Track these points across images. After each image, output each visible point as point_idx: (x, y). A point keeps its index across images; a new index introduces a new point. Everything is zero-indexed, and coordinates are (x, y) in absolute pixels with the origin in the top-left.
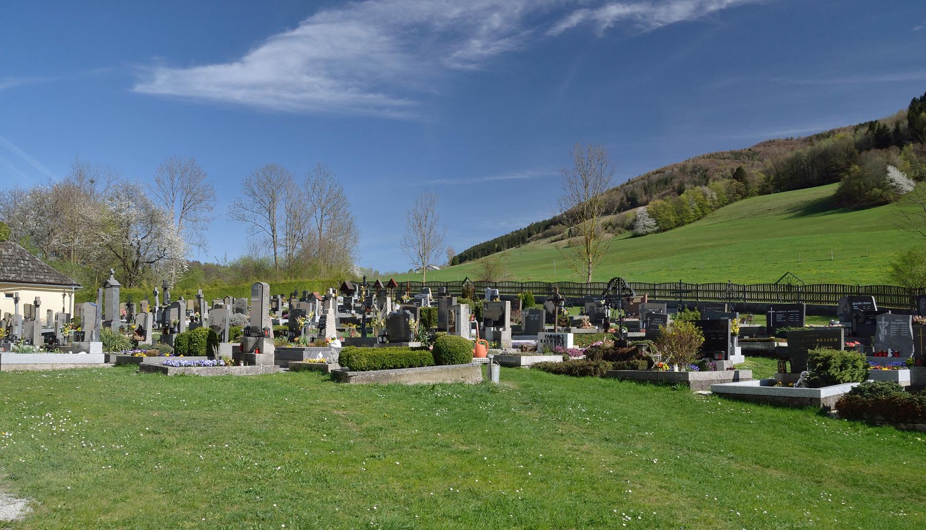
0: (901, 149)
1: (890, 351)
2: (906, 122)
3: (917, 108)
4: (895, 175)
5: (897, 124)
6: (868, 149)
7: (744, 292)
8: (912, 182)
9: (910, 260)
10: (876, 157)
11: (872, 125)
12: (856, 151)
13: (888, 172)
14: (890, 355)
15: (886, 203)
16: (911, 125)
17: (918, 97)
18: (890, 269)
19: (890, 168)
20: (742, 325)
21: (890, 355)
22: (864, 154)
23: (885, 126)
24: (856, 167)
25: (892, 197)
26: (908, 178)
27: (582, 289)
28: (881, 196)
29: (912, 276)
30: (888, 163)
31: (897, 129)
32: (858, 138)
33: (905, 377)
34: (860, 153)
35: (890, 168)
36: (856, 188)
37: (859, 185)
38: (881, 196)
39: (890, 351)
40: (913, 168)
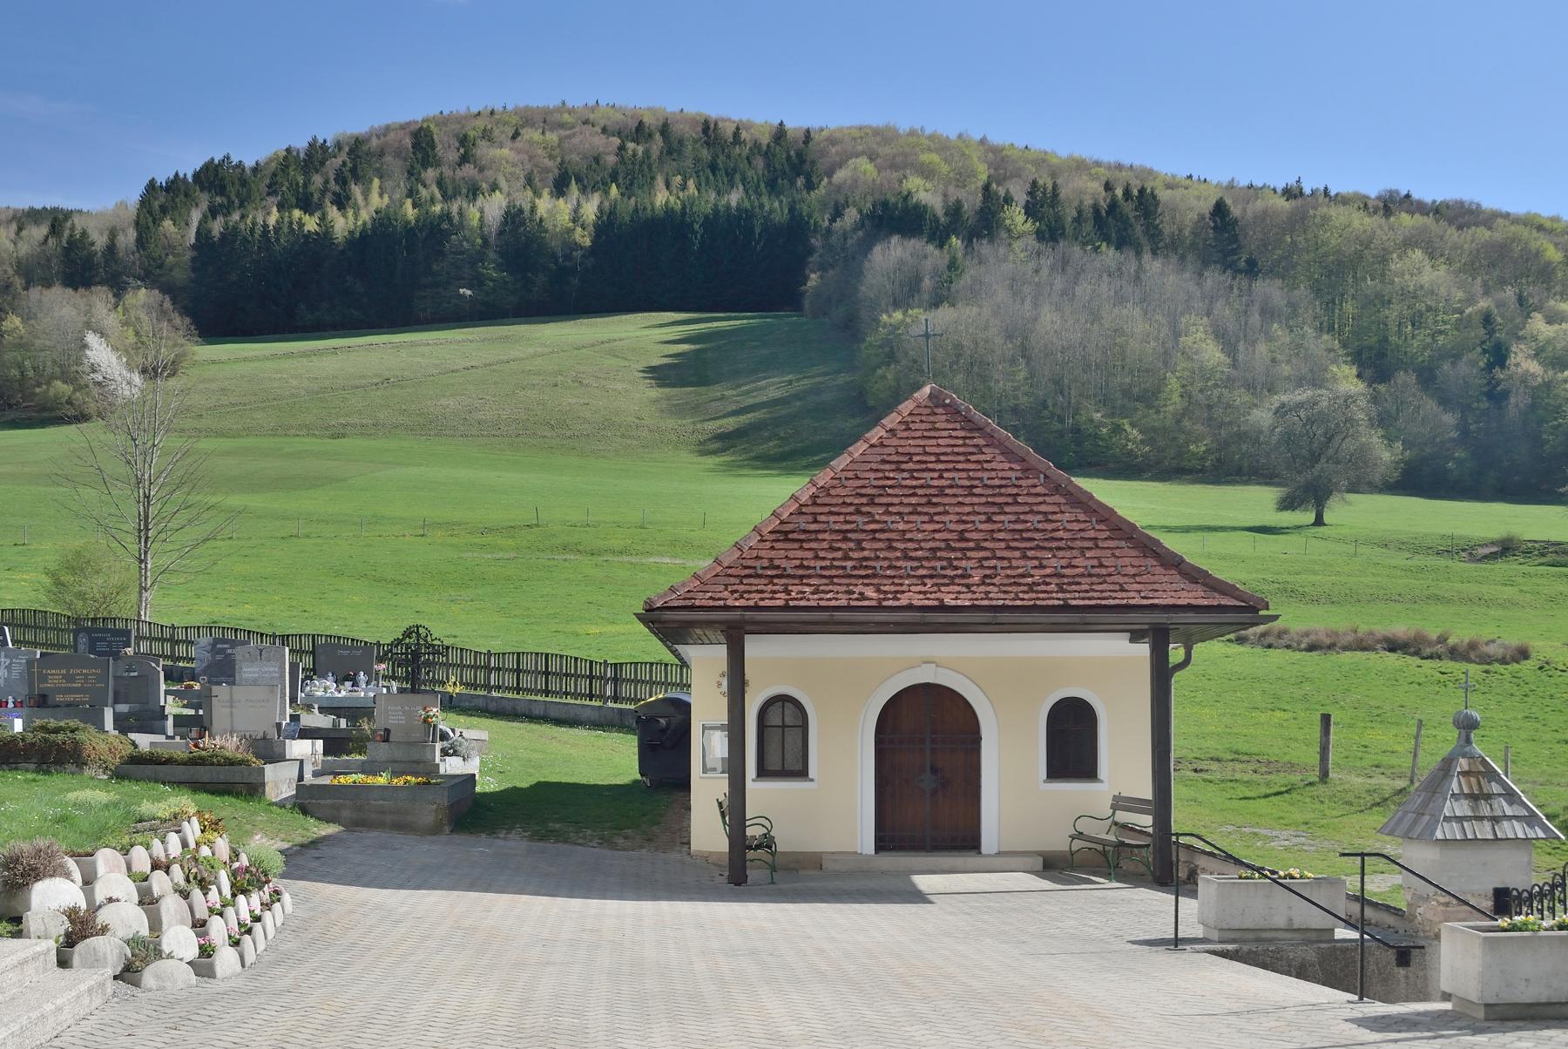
0: (118, 296)
1: (11, 700)
2: (132, 234)
3: (156, 204)
4: (101, 354)
5: (113, 234)
6: (48, 284)
7: (174, 642)
8: (137, 379)
9: (78, 565)
10: (60, 306)
11: (57, 220)
12: (18, 282)
13: (85, 346)
14: (11, 705)
15: (82, 418)
16: (141, 242)
17: (161, 179)
18: (47, 580)
19: (91, 338)
20: (524, 199)
21: (11, 705)
22: (35, 293)
23: (84, 234)
24: (17, 321)
25: (92, 408)
26: (130, 367)
27: (174, 642)
28: (69, 402)
29: (81, 596)
30: (88, 326)
31: (111, 248)
32: (24, 249)
33: (18, 725)
34: (26, 288)
35: (91, 338)
36: (15, 372)
37: (20, 366)
38: (69, 402)
39: (11, 700)
40: (140, 344)
